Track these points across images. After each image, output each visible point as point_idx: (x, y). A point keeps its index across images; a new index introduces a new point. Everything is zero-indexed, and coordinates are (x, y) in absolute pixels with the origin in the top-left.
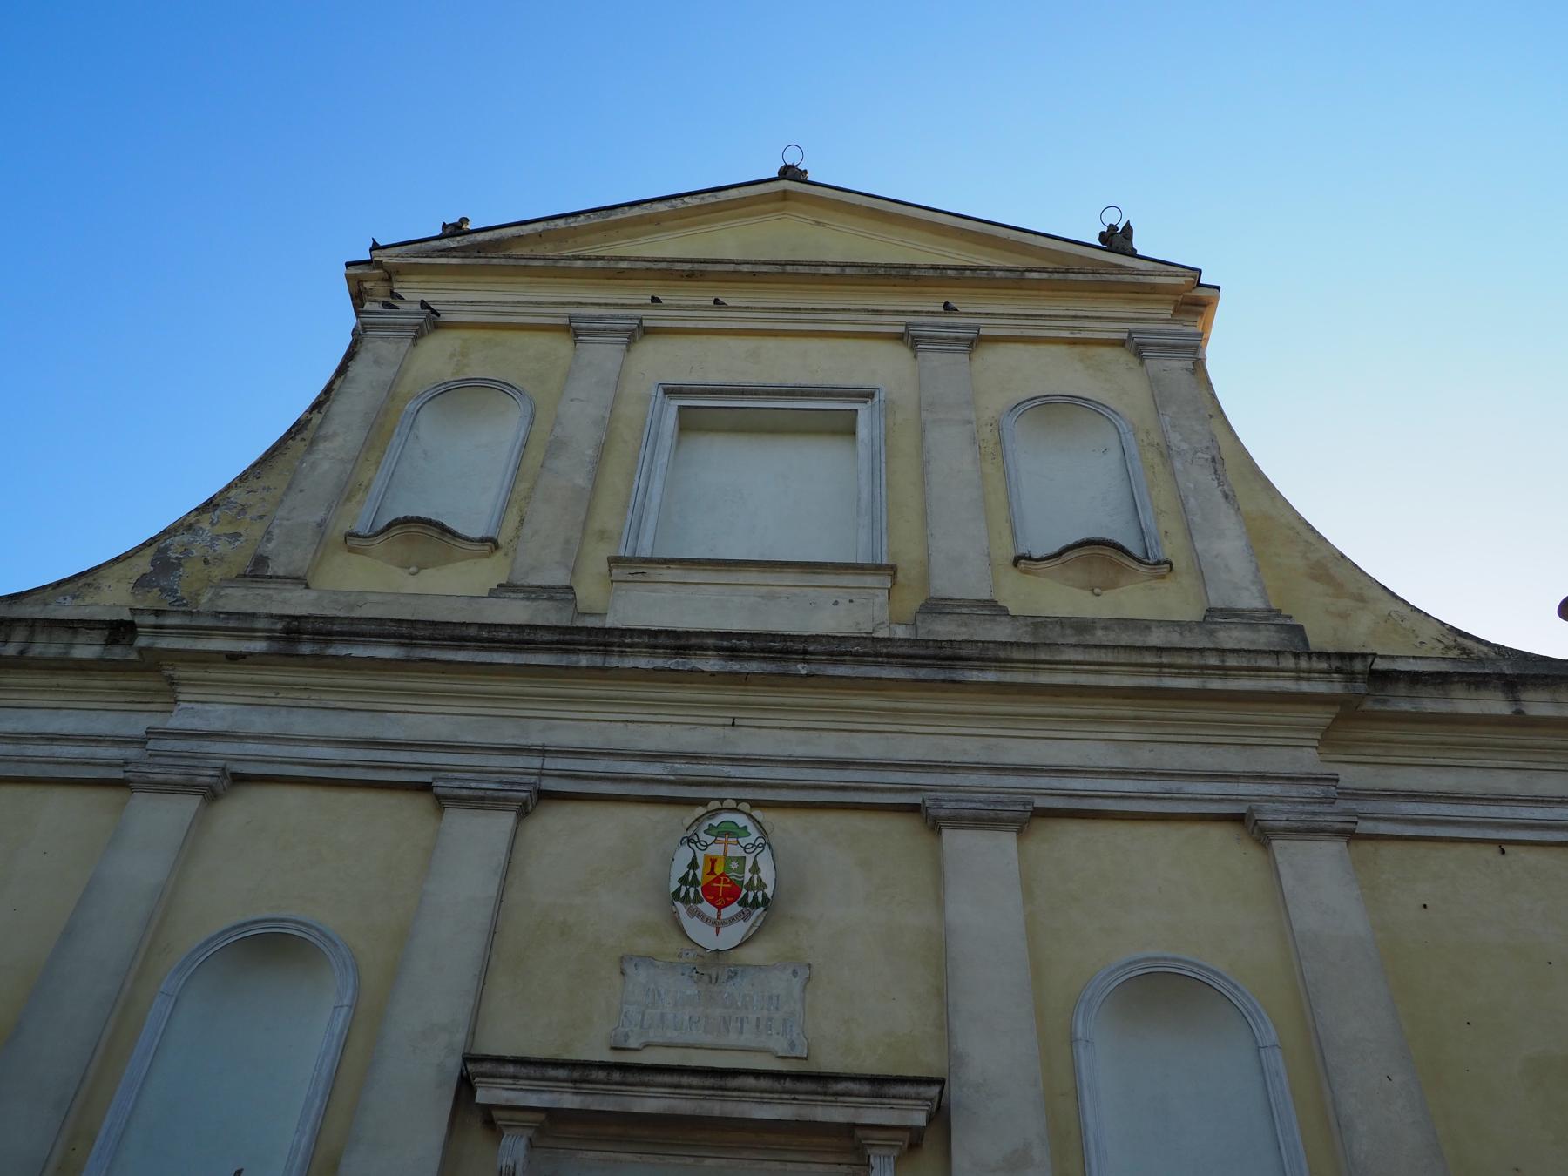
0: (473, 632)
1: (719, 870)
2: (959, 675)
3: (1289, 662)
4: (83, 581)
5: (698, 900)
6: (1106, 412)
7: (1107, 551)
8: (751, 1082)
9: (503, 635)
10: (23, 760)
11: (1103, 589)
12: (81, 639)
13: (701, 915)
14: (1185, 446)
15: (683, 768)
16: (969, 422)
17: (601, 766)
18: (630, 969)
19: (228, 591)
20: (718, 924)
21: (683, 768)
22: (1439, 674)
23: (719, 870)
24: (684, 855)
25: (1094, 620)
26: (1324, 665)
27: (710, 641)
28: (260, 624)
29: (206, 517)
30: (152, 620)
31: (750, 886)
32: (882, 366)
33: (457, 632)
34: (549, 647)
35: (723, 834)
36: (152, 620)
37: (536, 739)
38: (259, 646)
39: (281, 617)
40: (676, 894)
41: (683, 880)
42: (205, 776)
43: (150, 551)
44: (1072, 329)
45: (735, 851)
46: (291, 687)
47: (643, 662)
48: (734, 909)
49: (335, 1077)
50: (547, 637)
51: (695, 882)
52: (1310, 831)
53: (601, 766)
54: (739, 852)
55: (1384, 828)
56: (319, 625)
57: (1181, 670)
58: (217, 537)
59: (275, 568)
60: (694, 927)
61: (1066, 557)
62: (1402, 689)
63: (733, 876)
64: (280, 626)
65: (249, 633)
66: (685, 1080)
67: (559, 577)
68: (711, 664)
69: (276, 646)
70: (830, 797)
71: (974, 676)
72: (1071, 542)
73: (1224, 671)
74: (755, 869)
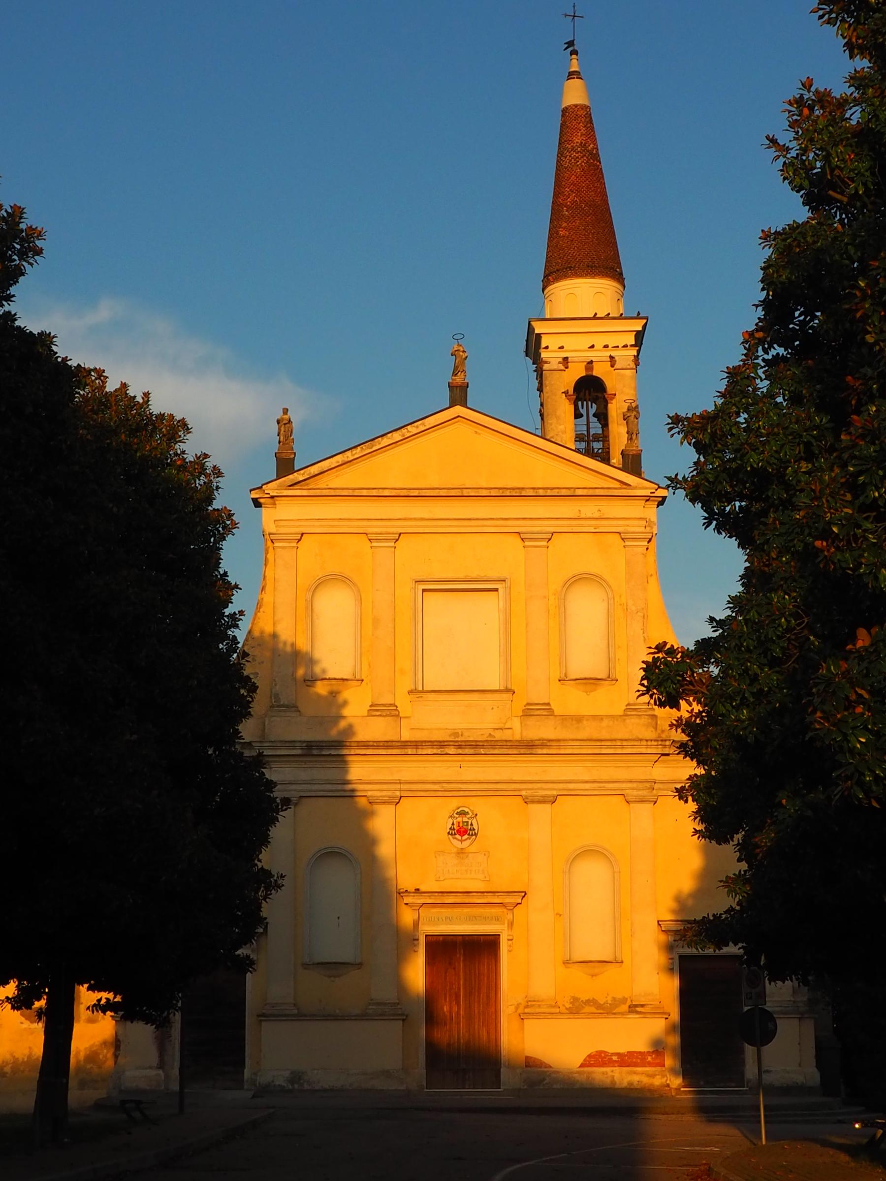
0: (371, 744)
2: (534, 751)
3: (644, 743)
6: (605, 584)
14: (634, 608)
16: (545, 597)
17: (419, 787)
20: (462, 841)
22: (603, 1064)
23: (461, 825)
24: (450, 821)
25: (583, 716)
26: (656, 743)
32: (503, 557)
34: (398, 747)
36: (259, 744)
37: (396, 777)
38: (299, 752)
39: (305, 742)
45: (465, 819)
47: (429, 751)
48: (466, 836)
53: (419, 787)
57: (608, 747)
60: (455, 842)
65: (294, 748)
69: (305, 752)
70: (493, 790)
71: (540, 751)
72: (578, 677)
73: (622, 747)
74: (472, 824)
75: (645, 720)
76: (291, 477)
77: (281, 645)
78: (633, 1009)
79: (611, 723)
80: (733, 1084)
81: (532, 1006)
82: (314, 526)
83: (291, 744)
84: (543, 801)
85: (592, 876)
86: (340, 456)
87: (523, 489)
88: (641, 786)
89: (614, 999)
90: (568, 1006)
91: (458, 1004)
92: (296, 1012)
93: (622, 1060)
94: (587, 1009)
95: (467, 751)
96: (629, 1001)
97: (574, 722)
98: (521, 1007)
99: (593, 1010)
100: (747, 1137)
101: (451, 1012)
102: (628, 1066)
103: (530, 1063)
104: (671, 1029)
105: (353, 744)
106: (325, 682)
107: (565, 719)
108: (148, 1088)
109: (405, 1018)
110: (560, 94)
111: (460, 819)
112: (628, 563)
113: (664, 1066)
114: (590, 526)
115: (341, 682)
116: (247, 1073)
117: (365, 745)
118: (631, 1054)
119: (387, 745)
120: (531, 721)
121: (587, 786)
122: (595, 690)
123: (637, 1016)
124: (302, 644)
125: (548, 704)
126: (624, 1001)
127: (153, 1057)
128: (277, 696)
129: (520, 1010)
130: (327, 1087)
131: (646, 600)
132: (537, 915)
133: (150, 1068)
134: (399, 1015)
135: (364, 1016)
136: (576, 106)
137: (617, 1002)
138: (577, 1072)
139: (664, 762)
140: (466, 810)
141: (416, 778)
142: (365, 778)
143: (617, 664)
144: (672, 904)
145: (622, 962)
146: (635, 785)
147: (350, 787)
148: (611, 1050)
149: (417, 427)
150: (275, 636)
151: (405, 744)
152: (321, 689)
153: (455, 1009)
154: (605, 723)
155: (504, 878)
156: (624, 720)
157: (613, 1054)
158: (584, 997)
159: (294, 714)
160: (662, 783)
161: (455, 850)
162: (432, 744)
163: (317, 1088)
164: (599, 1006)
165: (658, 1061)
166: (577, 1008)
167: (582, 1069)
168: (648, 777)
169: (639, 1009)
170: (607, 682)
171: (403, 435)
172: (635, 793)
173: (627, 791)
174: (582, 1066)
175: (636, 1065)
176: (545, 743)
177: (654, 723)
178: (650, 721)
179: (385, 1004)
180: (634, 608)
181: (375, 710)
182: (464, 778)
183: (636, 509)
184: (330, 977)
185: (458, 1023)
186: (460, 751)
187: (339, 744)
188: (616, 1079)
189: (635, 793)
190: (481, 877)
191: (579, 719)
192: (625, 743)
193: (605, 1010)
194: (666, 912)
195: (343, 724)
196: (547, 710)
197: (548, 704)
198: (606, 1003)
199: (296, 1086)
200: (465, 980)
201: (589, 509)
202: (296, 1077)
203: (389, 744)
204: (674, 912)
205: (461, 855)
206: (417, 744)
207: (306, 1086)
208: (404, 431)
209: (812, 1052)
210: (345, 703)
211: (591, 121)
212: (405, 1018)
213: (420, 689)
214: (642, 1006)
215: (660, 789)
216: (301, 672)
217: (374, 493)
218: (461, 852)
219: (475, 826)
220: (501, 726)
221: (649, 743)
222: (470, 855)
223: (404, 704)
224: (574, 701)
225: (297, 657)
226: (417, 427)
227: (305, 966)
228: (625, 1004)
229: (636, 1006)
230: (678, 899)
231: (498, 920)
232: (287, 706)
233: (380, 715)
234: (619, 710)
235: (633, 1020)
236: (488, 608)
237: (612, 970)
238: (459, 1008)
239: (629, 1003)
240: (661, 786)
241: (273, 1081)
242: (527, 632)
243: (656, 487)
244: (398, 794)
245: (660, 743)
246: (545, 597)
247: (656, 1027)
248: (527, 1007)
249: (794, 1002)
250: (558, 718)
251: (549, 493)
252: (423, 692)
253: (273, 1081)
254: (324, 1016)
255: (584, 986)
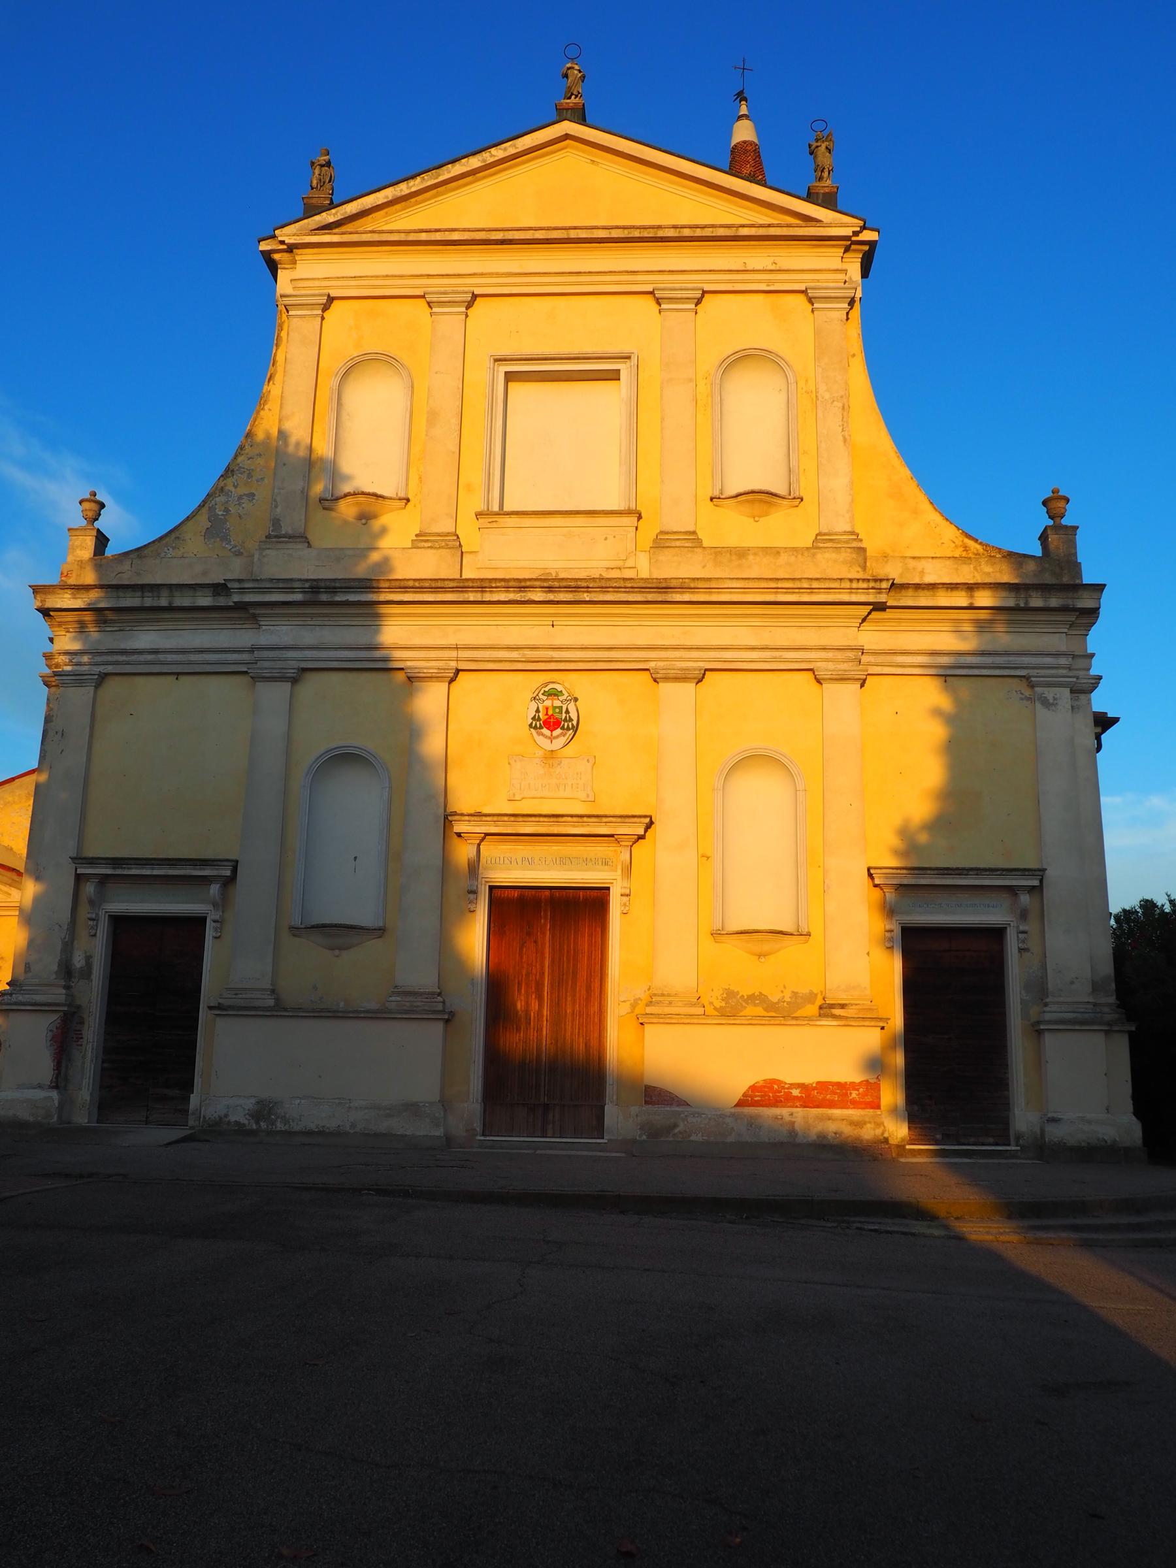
0: (411, 584)
1: (550, 713)
3: (847, 584)
4: (173, 536)
5: (541, 727)
6: (782, 363)
7: (763, 496)
8: (569, 819)
9: (427, 585)
10: (190, 663)
11: (760, 517)
12: (198, 594)
13: (543, 735)
14: (827, 396)
15: (530, 654)
16: (691, 380)
18: (512, 762)
19: (268, 552)
20: (551, 739)
21: (530, 654)
22: (776, 1103)
23: (550, 713)
24: (534, 706)
25: (749, 549)
26: (865, 585)
27: (537, 583)
28: (296, 585)
29: (229, 481)
30: (236, 585)
31: (565, 720)
33: (402, 584)
34: (453, 590)
35: (550, 695)
36: (236, 585)
37: (452, 640)
38: (298, 597)
39: (307, 580)
40: (531, 726)
41: (533, 718)
42: (291, 673)
43: (205, 510)
44: (769, 282)
45: (557, 703)
46: (320, 615)
47: (503, 597)
48: (558, 731)
49: (389, 820)
50: (452, 584)
51: (539, 719)
52: (842, 679)
54: (559, 704)
55: (886, 670)
56: (328, 584)
58: (240, 498)
59: (286, 529)
60: (540, 740)
61: (740, 499)
62: (910, 592)
63: (557, 716)
64: (307, 585)
65: (291, 590)
66: (541, 819)
67: (446, 526)
68: (538, 596)
69: (308, 597)
70: (603, 663)
72: (741, 490)
74: (567, 712)
75: (845, 555)
76: (317, 218)
77: (291, 449)
78: (827, 1010)
79: (793, 559)
80: (991, 1140)
81: (658, 1003)
82: (348, 287)
83: (287, 585)
84: (681, 678)
85: (761, 800)
86: (391, 189)
87: (659, 227)
88: (839, 655)
89: (795, 994)
90: (718, 1004)
91: (540, 998)
92: (271, 1002)
93: (808, 1096)
94: (750, 1010)
95: (562, 597)
96: (820, 998)
97: (734, 557)
98: (641, 1004)
99: (759, 1011)
100: (1161, 1291)
101: (527, 1012)
102: (818, 1107)
103: (654, 1095)
104: (890, 1045)
105: (383, 585)
106: (349, 499)
107: (717, 552)
108: (31, 1119)
109: (449, 1019)
110: (730, 134)
111: (548, 703)
112: (817, 333)
113: (878, 1107)
114: (760, 282)
115: (373, 499)
116: (194, 1100)
117: (403, 586)
118: (823, 1086)
119: (436, 585)
120: (665, 556)
121: (754, 655)
122: (766, 514)
123: (835, 1023)
124: (323, 448)
125: (694, 533)
126: (811, 998)
127: (45, 1068)
128: (276, 522)
129: (638, 1011)
130: (313, 1127)
131: (847, 384)
132: (669, 856)
133: (40, 1086)
134: (435, 1012)
135: (379, 1015)
136: (745, 142)
137: (800, 1001)
138: (733, 1115)
139: (877, 621)
140: (559, 688)
141: (786, 644)
142: (402, 643)
143: (802, 479)
144: (894, 841)
145: (809, 934)
146: (830, 655)
147: (378, 654)
148: (789, 1080)
149: (505, 149)
150: (283, 435)
151: (463, 585)
152: (347, 510)
153: (535, 1005)
154: (784, 558)
155: (618, 795)
156: (814, 555)
157: (793, 1086)
158: (745, 992)
159: (300, 546)
160: (875, 653)
161: (540, 753)
162: (506, 584)
163: (297, 1128)
164: (771, 1006)
165: (868, 1099)
166: (732, 1009)
167: (739, 1109)
168: (852, 643)
169: (837, 1012)
170: (785, 502)
171: (484, 161)
172: (831, 666)
173: (819, 664)
174: (739, 1104)
175: (831, 1105)
176: (684, 586)
177: (861, 559)
178: (854, 556)
179: (414, 994)
180: (827, 396)
181: (422, 539)
182: (558, 642)
183: (831, 258)
184: (332, 949)
185: (539, 1030)
186: (551, 597)
187: (367, 585)
188: (797, 1127)
189: (831, 666)
190: (583, 796)
191: (741, 553)
192: (815, 585)
193: (781, 1012)
194: (897, 821)
195: (375, 557)
196: (693, 540)
197: (694, 533)
198: (782, 1000)
199: (263, 1125)
200: (553, 962)
201: (758, 258)
202: (264, 1110)
203: (439, 584)
204: (896, 853)
205: (551, 762)
206: (482, 585)
207: (280, 1126)
208: (485, 155)
209: (1128, 1089)
210: (384, 531)
211: (759, 156)
212: (449, 1019)
213: (496, 508)
214: (843, 1006)
215: (869, 664)
216: (318, 488)
217: (438, 236)
218: (551, 755)
219: (573, 715)
220: (620, 564)
221: (855, 585)
222: (565, 762)
223: (469, 532)
224: (735, 528)
225: (310, 465)
226: (505, 149)
227: (295, 931)
228: (813, 1003)
229: (832, 1006)
230: (904, 832)
231: (606, 864)
232: (290, 537)
233: (431, 547)
234: (805, 539)
235: (828, 1030)
236: (606, 400)
237: (792, 950)
238: (541, 1005)
239: (819, 1001)
240: (872, 659)
241: (226, 1116)
242: (662, 429)
243: (861, 223)
244: (453, 664)
245: (872, 584)
246: (691, 380)
247: (870, 1039)
248: (649, 1004)
249: (1095, 1005)
250: (708, 551)
251: (699, 233)
252: (502, 513)
253: (226, 1116)
254: (313, 1011)
255: (742, 970)
